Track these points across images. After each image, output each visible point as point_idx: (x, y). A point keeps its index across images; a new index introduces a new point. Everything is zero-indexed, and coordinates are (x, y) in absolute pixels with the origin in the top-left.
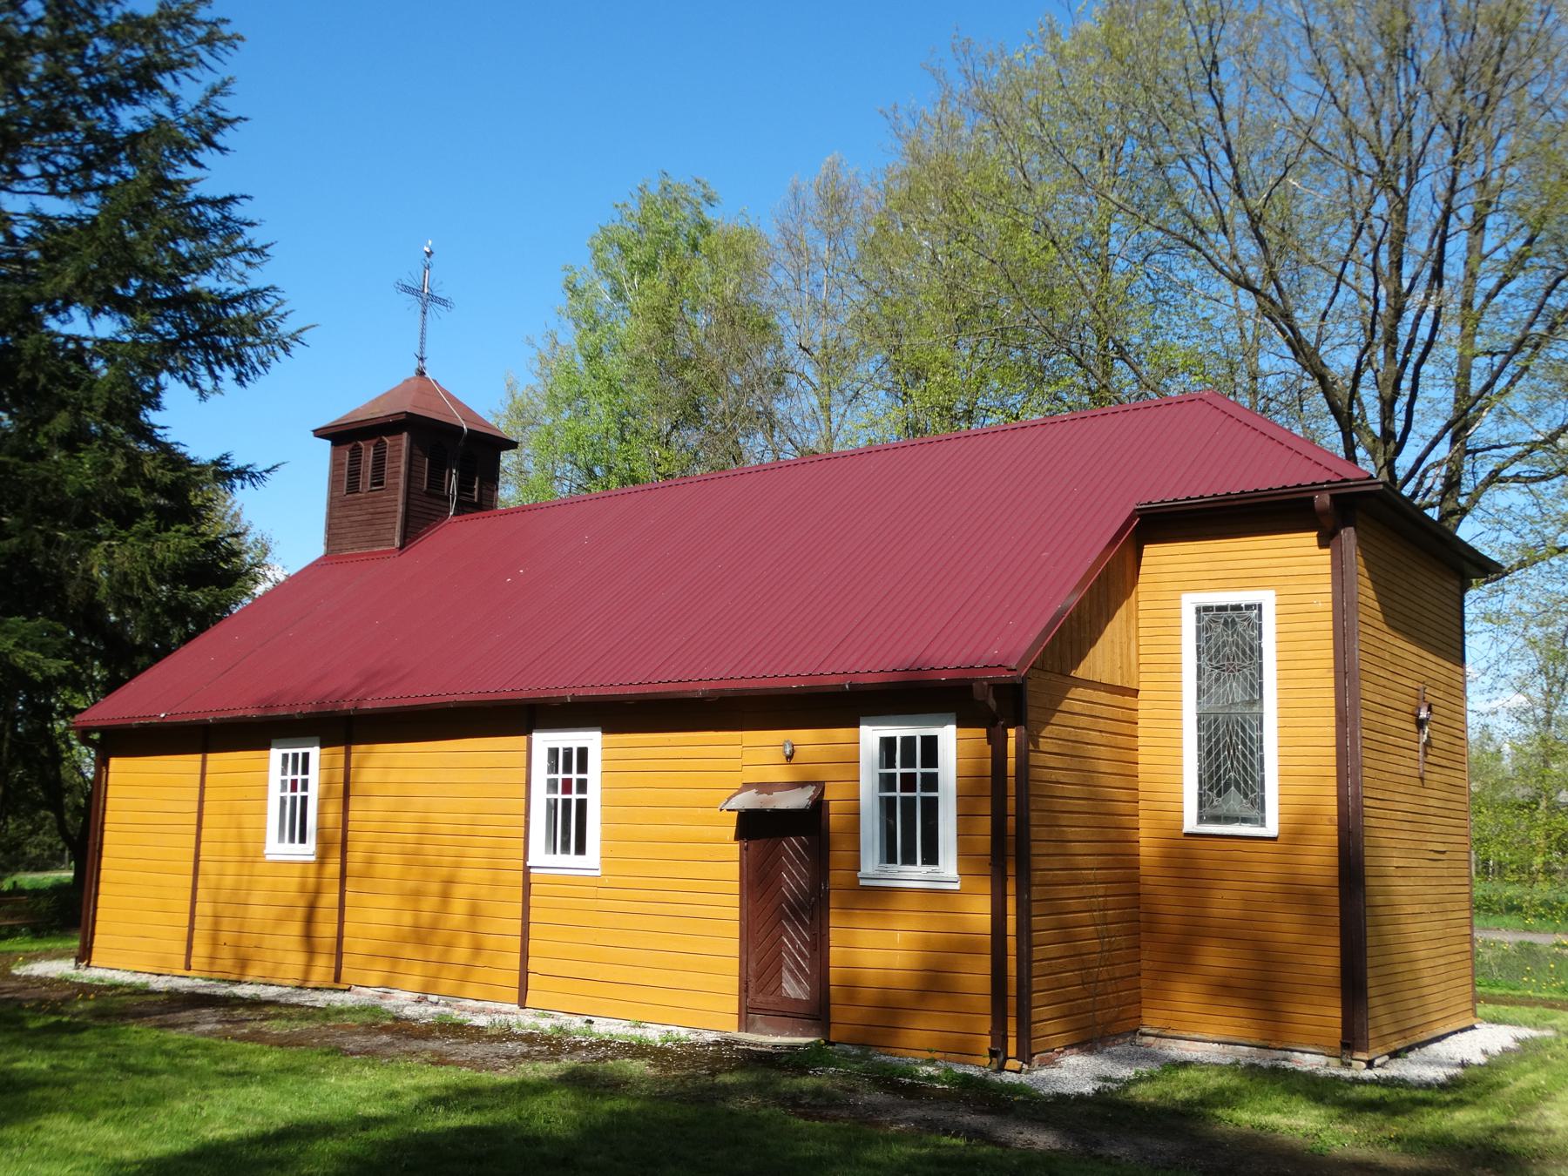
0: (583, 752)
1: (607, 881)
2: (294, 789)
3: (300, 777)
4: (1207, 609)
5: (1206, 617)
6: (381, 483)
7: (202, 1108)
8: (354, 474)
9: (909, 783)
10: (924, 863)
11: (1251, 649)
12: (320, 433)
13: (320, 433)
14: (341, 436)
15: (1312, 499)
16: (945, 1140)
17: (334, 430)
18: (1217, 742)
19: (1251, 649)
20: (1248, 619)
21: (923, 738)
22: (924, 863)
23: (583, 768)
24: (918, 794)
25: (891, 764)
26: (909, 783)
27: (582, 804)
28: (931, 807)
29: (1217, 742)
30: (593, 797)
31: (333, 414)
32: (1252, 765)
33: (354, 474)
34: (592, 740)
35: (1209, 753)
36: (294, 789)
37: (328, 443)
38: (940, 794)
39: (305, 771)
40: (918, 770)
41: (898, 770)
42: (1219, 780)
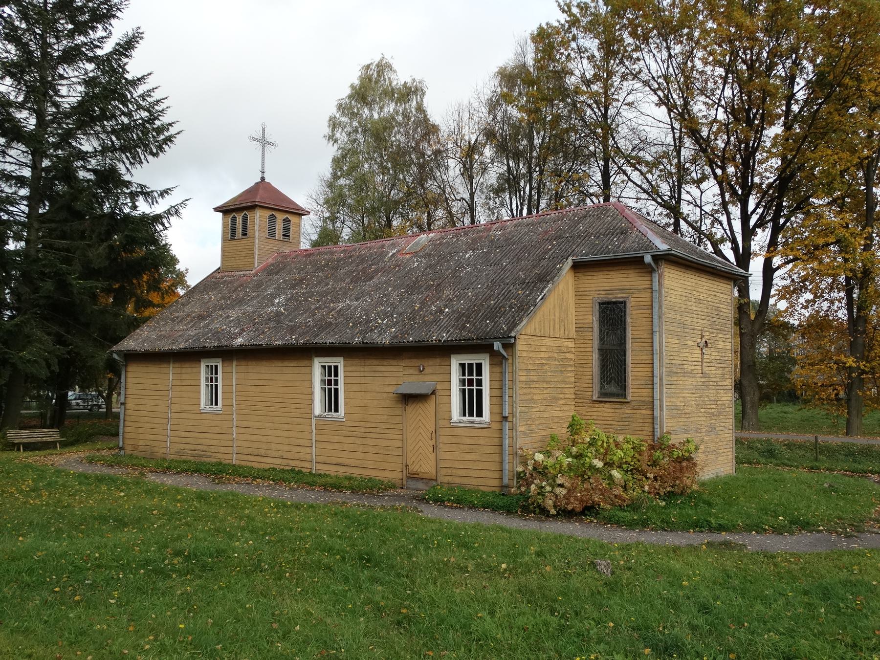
0: (336, 368)
1: (348, 424)
2: (212, 381)
3: (214, 376)
4: (603, 303)
5: (603, 306)
6: (246, 234)
7: (58, 539)
8: (234, 230)
9: (470, 382)
10: (477, 416)
11: (621, 321)
12: (217, 209)
13: (217, 209)
14: (225, 210)
15: (643, 257)
16: (754, 542)
17: (224, 209)
18: (607, 362)
19: (621, 321)
20: (620, 308)
21: (476, 364)
22: (477, 416)
23: (336, 375)
24: (475, 388)
25: (464, 375)
26: (470, 382)
27: (336, 390)
28: (480, 393)
29: (607, 362)
30: (341, 387)
31: (219, 203)
32: (621, 372)
33: (234, 230)
34: (339, 362)
35: (604, 366)
36: (212, 381)
37: (221, 214)
38: (483, 388)
39: (216, 374)
40: (474, 377)
41: (466, 377)
42: (607, 378)
